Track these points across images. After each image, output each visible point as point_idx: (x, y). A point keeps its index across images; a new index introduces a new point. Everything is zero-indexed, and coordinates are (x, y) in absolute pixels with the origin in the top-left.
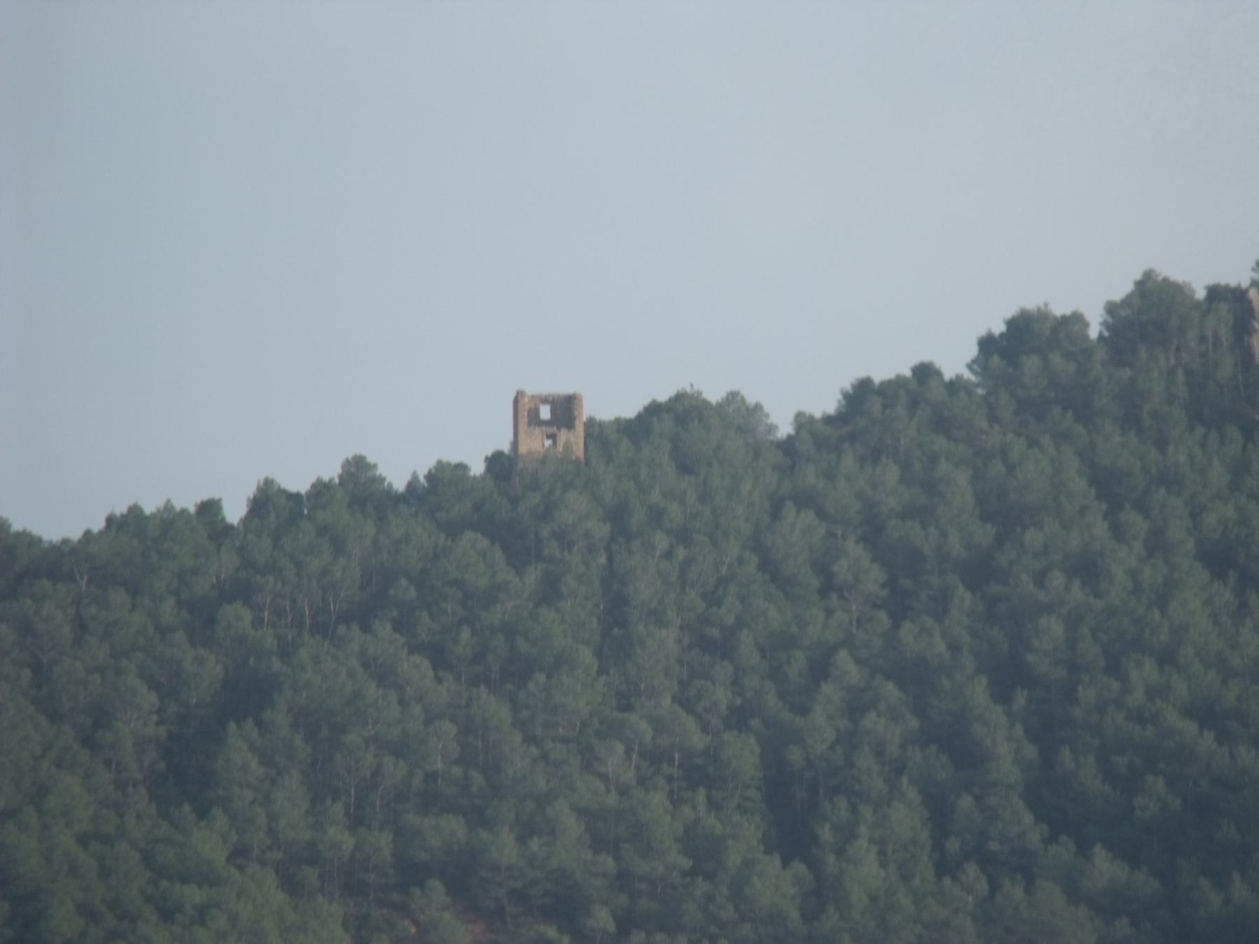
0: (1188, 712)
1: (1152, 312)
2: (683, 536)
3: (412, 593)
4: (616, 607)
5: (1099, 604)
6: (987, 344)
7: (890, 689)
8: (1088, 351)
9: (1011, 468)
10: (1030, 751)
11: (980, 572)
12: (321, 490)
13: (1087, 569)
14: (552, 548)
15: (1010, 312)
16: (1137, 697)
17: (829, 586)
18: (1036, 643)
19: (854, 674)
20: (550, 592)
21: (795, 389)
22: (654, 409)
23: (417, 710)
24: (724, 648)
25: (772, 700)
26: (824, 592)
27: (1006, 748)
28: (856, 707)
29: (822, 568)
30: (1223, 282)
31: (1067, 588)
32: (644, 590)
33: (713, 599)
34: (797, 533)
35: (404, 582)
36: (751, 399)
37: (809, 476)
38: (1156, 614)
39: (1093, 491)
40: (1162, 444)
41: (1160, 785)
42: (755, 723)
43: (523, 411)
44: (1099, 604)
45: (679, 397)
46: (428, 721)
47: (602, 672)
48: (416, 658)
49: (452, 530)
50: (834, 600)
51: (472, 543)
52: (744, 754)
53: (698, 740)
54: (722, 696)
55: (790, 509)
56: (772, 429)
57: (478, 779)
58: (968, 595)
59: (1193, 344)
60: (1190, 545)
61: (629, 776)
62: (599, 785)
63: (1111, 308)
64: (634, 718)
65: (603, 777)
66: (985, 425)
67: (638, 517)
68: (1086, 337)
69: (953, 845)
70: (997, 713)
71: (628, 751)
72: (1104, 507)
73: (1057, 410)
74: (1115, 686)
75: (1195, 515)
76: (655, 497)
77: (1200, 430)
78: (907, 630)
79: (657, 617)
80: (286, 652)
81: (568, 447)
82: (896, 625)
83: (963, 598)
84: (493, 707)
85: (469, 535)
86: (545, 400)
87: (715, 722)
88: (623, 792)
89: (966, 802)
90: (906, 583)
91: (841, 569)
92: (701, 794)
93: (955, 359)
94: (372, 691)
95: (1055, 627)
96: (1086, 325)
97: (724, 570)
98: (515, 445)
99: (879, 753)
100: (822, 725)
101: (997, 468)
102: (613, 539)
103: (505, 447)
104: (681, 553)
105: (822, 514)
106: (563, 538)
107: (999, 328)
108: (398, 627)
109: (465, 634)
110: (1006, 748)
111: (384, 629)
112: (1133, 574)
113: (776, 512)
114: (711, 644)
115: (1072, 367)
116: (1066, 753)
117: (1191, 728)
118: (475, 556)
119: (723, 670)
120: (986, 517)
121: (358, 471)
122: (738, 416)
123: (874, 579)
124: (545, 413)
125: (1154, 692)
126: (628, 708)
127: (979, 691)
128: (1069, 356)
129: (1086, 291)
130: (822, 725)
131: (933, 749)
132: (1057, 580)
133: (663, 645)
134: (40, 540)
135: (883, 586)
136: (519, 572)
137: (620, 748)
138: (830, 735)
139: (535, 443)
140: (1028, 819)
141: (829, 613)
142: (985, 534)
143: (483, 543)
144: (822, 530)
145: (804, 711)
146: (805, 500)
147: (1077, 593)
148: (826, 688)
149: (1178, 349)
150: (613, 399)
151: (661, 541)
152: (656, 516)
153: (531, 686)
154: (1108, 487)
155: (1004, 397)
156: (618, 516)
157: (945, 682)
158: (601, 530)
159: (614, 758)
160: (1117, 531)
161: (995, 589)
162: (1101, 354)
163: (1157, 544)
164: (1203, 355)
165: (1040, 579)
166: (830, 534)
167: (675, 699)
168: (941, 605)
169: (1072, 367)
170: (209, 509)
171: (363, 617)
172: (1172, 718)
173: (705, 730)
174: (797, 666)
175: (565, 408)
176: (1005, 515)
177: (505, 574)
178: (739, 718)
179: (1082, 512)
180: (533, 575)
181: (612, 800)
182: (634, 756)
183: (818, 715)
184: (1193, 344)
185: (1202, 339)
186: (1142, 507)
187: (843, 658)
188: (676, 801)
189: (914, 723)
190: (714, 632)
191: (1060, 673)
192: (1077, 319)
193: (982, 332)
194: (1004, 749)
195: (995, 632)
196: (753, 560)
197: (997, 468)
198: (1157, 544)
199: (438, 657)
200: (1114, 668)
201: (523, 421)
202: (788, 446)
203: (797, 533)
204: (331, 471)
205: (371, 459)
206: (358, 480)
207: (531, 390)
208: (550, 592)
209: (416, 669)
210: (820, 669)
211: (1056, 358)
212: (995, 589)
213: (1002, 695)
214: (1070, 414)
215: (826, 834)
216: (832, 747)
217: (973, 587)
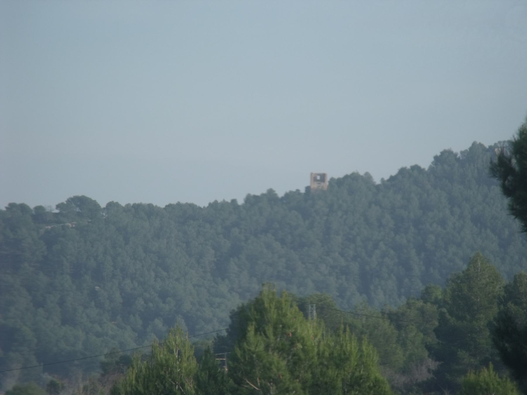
7: (392, 252)
15: (442, 150)
21: (381, 171)
22: (346, 177)
30: (373, 178)
43: (314, 179)
45: (353, 174)
69: (403, 290)
86: (318, 175)
89: (406, 280)
92: (344, 277)
93: (426, 163)
95: (432, 237)
107: (439, 154)
121: (271, 192)
122: (368, 178)
124: (318, 178)
134: (196, 206)
139: (315, 186)
170: (234, 201)
187: (381, 244)
204: (265, 191)
206: (270, 195)
215: (372, 287)
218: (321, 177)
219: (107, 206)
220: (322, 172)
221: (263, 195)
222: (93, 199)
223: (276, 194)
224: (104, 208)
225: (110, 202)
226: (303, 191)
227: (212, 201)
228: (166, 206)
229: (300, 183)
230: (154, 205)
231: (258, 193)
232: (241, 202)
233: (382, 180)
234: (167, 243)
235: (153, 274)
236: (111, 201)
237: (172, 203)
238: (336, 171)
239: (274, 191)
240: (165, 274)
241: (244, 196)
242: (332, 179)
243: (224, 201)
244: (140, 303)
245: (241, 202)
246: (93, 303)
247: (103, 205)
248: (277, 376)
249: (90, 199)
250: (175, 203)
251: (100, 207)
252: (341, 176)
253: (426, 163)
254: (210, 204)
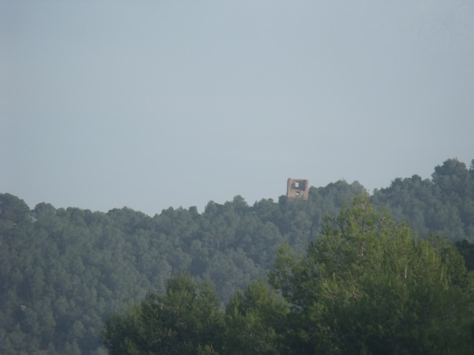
3: (250, 240)
15: (445, 160)
21: (374, 180)
22: (331, 185)
23: (249, 275)
35: (248, 236)
43: (291, 184)
45: (339, 182)
48: (250, 260)
49: (264, 221)
80: (211, 256)
81: (303, 196)
86: (297, 181)
93: (427, 174)
94: (235, 269)
98: (287, 193)
107: (441, 164)
108: (245, 250)
109: (265, 253)
111: (240, 250)
122: (357, 188)
124: (297, 185)
136: (283, 235)
139: (293, 194)
143: (273, 225)
158: (309, 223)
162: (469, 176)
170: (193, 209)
171: (234, 246)
193: (436, 165)
197: (432, 210)
201: (290, 189)
204: (231, 199)
205: (243, 197)
207: (294, 177)
208: (292, 241)
211: (455, 177)
218: (299, 185)
219: (36, 208)
220: (302, 178)
221: (228, 204)
222: (20, 198)
223: (245, 203)
224: (33, 211)
225: (40, 204)
226: (276, 201)
227: (166, 208)
228: (110, 211)
229: (275, 191)
230: (93, 211)
231: (222, 202)
232: (201, 210)
233: (375, 190)
234: (113, 255)
235: (95, 292)
236: (41, 202)
237: (118, 208)
238: (319, 178)
240: (109, 292)
242: (312, 188)
243: (181, 208)
244: (79, 327)
245: (201, 210)
246: (18, 326)
247: (32, 207)
249: (16, 197)
250: (121, 208)
251: (28, 208)
252: (324, 185)
253: (427, 174)
254: (163, 211)
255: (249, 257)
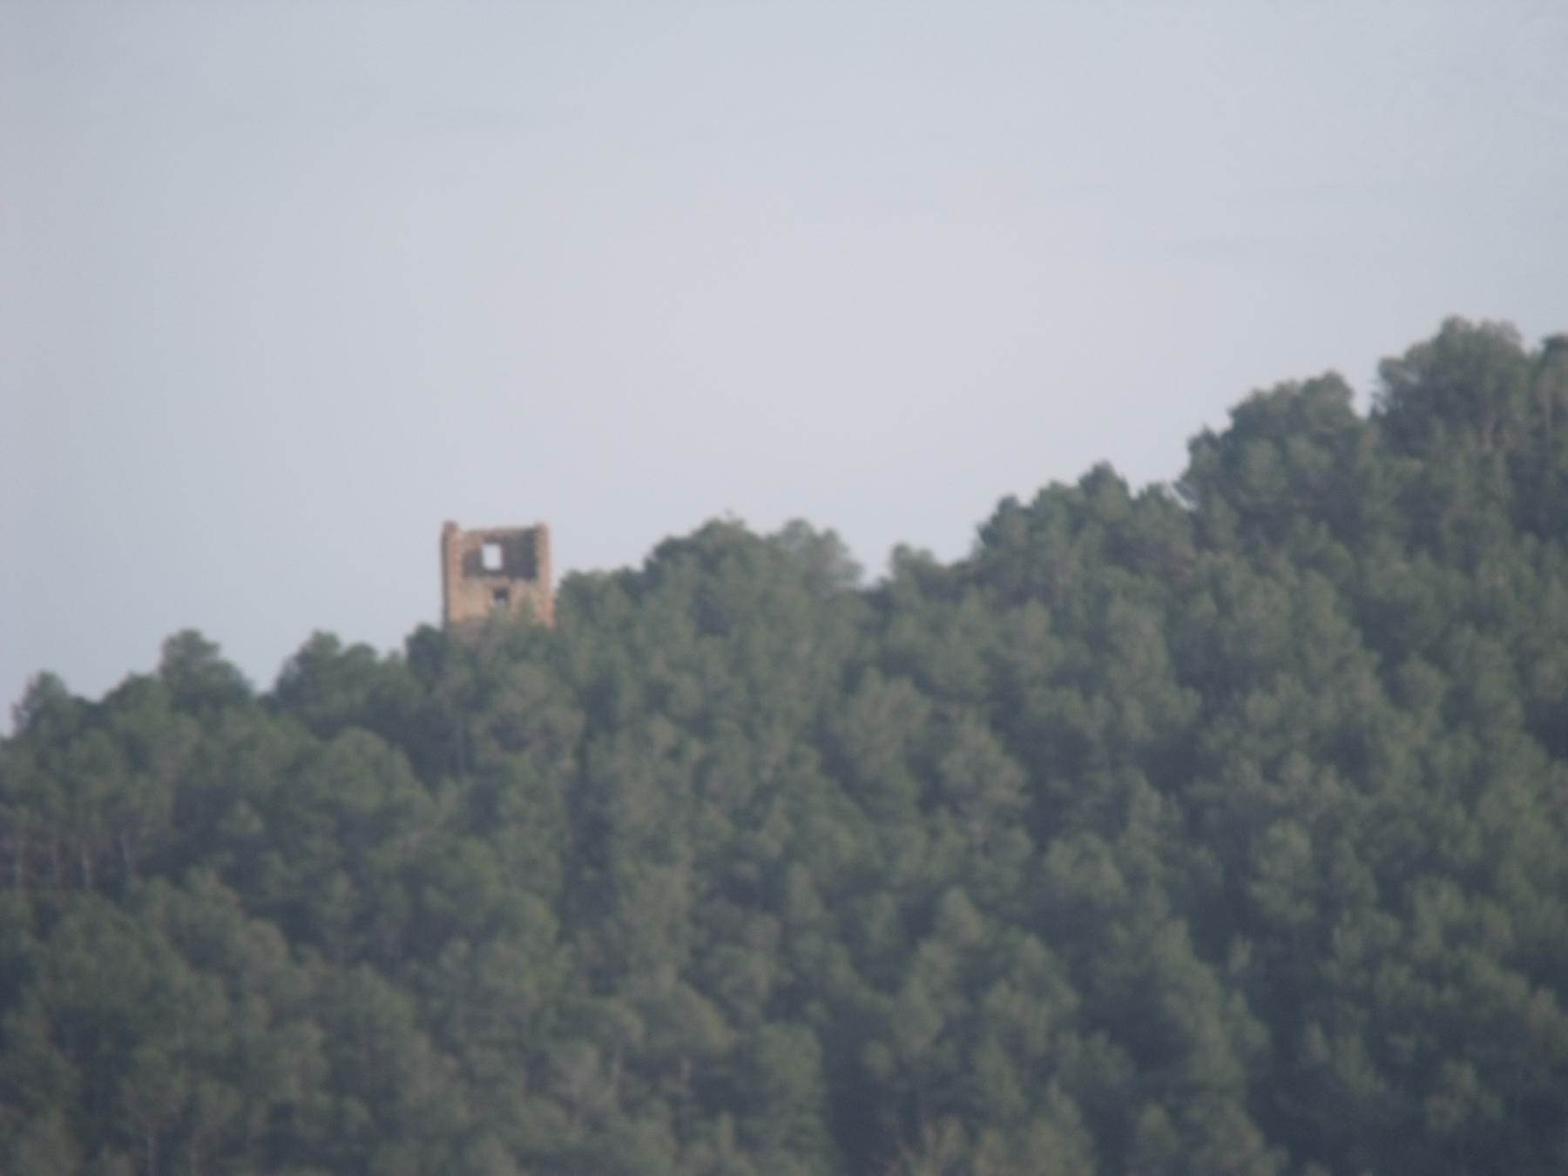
0: (1512, 962)
1: (1455, 378)
2: (701, 725)
3: (257, 825)
4: (590, 837)
5: (1366, 804)
6: (1202, 444)
7: (1033, 950)
8: (1352, 432)
9: (1225, 606)
10: (1258, 1034)
11: (1176, 763)
12: (131, 692)
13: (1350, 752)
14: (490, 752)
15: (1238, 394)
16: (1429, 941)
17: (936, 795)
18: (1265, 866)
19: (974, 927)
20: (483, 816)
22: (669, 550)
23: (258, 1007)
24: (764, 894)
25: (842, 971)
26: (927, 804)
27: (1217, 1028)
28: (977, 975)
29: (924, 767)
31: (1315, 781)
32: (636, 807)
33: (746, 819)
34: (884, 717)
35: (242, 809)
36: (819, 526)
37: (907, 631)
38: (1459, 813)
39: (1357, 635)
40: (1468, 565)
41: (1466, 1077)
42: (814, 1008)
43: (460, 557)
44: (1366, 804)
46: (279, 1017)
47: (563, 936)
48: (260, 926)
49: (327, 729)
50: (943, 816)
51: (360, 746)
52: (794, 1057)
53: (717, 1035)
54: (761, 969)
55: (873, 681)
56: (853, 570)
57: (358, 1111)
58: (1155, 798)
59: (1520, 416)
60: (1515, 710)
61: (606, 1097)
62: (557, 1114)
63: (1388, 370)
64: (614, 1005)
65: (568, 1104)
66: (1190, 552)
67: (628, 699)
68: (1347, 412)
70: (1203, 976)
71: (606, 1058)
72: (1376, 657)
73: (1302, 523)
74: (1392, 926)
75: (1524, 664)
76: (657, 667)
77: (1530, 541)
78: (1060, 856)
79: (656, 849)
80: (45, 920)
81: (526, 607)
82: (1042, 848)
83: (1148, 801)
84: (385, 999)
85: (353, 734)
86: (492, 538)
87: (750, 1009)
88: (596, 1124)
89: (1153, 1117)
90: (1059, 785)
91: (955, 767)
92: (725, 1126)
94: (181, 975)
95: (1296, 840)
96: (1347, 393)
97: (767, 775)
98: (446, 610)
99: (1015, 1045)
100: (921, 1008)
101: (1205, 605)
102: (589, 734)
103: (434, 619)
104: (696, 749)
105: (924, 684)
106: (508, 735)
108: (234, 877)
109: (341, 885)
110: (1217, 1028)
111: (206, 881)
112: (1423, 757)
113: (851, 680)
114: (741, 889)
115: (1325, 458)
116: (1315, 1036)
117: (1516, 986)
118: (364, 769)
119: (763, 928)
120: (1185, 679)
122: (808, 555)
123: (1007, 779)
124: (492, 557)
125: (1455, 935)
126: (609, 991)
127: (1175, 945)
128: (1322, 441)
129: (1355, 345)
130: (921, 1008)
131: (1100, 1039)
132: (1299, 768)
133: (663, 892)
135: (1024, 790)
136: (432, 786)
137: (590, 1055)
138: (935, 1023)
139: (476, 603)
140: (1254, 1140)
141: (934, 833)
142: (1183, 705)
143: (375, 744)
144: (923, 707)
145: (891, 986)
146: (894, 664)
147: (1332, 787)
148: (931, 950)
149: (1497, 429)
150: (600, 539)
151: (663, 732)
152: (657, 698)
153: (446, 960)
154: (1384, 629)
155: (1220, 508)
156: (597, 701)
157: (1119, 933)
158: (570, 721)
159: (581, 1068)
160: (1398, 694)
161: (1200, 789)
162: (1372, 438)
163: (1461, 710)
164: (1538, 433)
165: (1271, 770)
166: (939, 718)
167: (683, 975)
168: (1113, 819)
169: (1325, 458)
171: (173, 865)
172: (1487, 972)
173: (734, 1020)
174: (881, 916)
175: (524, 551)
176: (1214, 673)
177: (408, 789)
178: (787, 1002)
179: (1340, 665)
180: (452, 795)
181: (575, 1136)
182: (616, 1068)
183: (916, 991)
184: (1520, 416)
185: (1536, 409)
186: (1437, 657)
187: (956, 903)
188: (682, 1133)
189: (1070, 999)
190: (748, 870)
191: (1305, 911)
192: (1330, 387)
193: (1195, 430)
194: (1213, 1033)
195: (1203, 855)
196: (812, 759)
197: (1205, 605)
198: (1461, 710)
199: (299, 926)
200: (1394, 901)
201: (456, 577)
202: (882, 600)
203: (884, 717)
204: (147, 661)
205: (209, 636)
206: (192, 678)
207: (472, 520)
208: (483, 816)
209: (260, 944)
210: (919, 920)
211: (1301, 447)
212: (1200, 789)
213: (1211, 947)
214: (1323, 529)
216: (938, 1041)
217: (1165, 784)
218: (506, 556)
220: (517, 519)
239: (210, 648)
241: (292, 641)
248: (976, 747)
255: (254, 911)
